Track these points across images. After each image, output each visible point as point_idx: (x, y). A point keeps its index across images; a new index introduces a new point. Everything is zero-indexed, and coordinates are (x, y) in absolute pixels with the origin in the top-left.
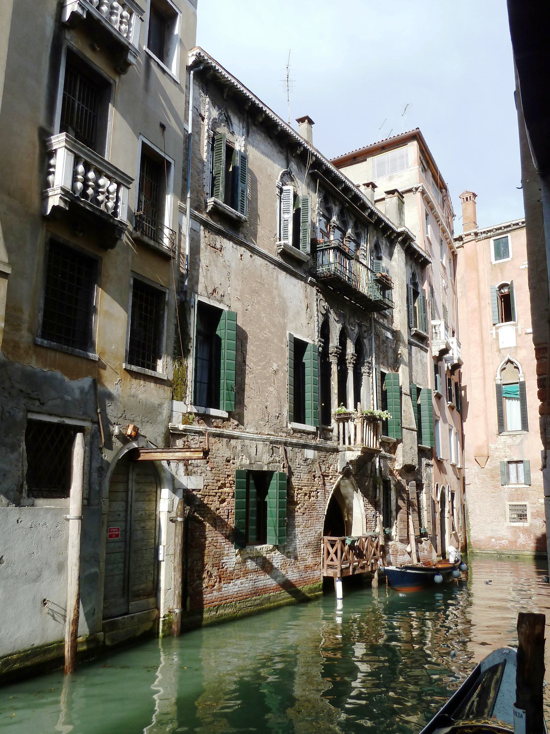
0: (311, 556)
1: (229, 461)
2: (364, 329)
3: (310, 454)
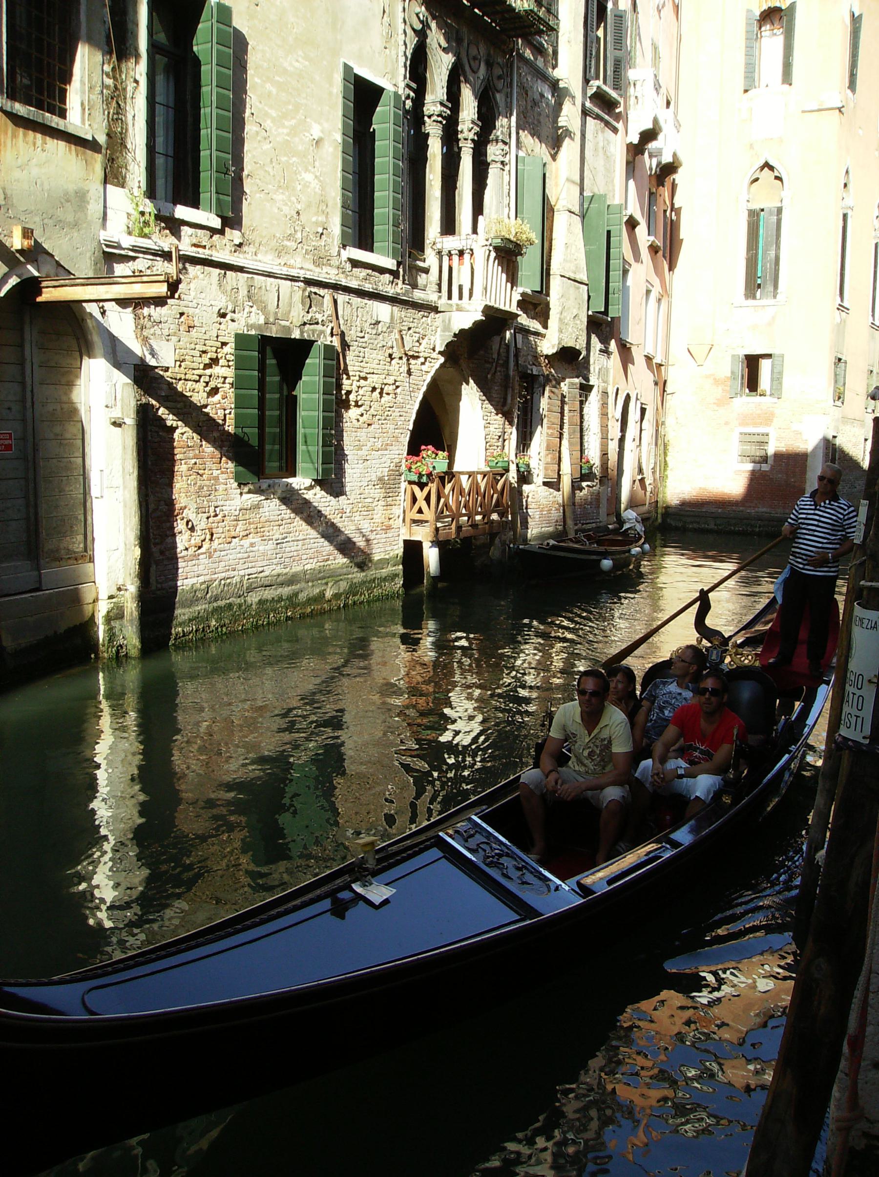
0: (381, 503)
1: (223, 316)
2: (498, 71)
3: (383, 311)
